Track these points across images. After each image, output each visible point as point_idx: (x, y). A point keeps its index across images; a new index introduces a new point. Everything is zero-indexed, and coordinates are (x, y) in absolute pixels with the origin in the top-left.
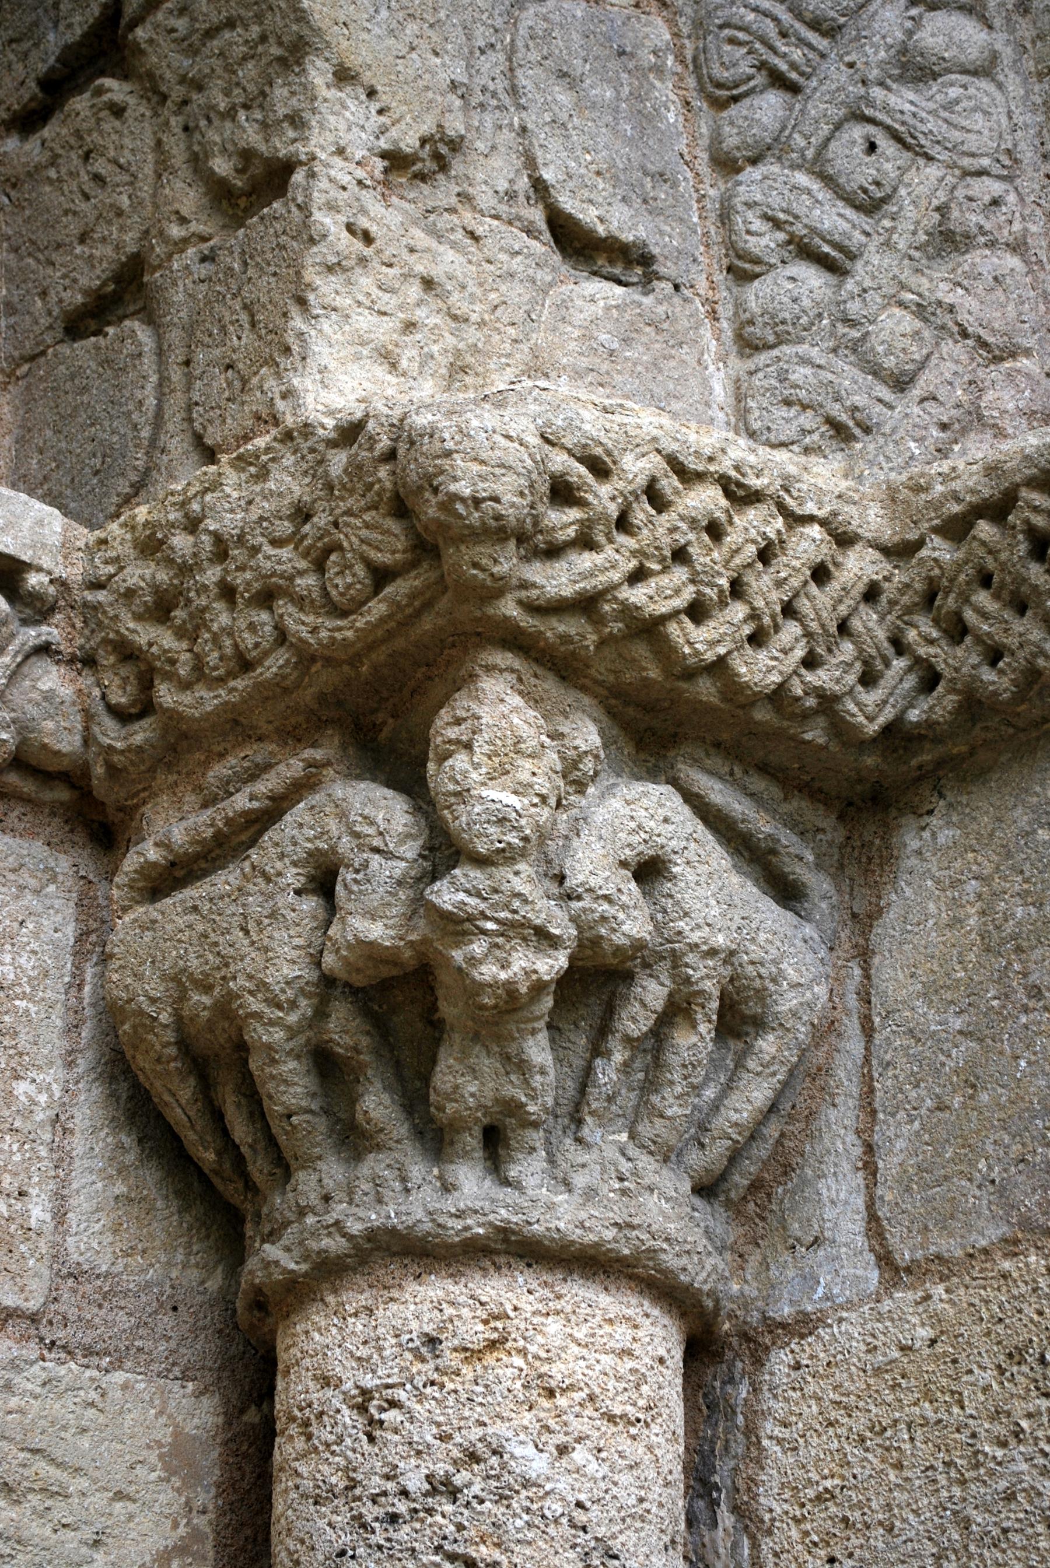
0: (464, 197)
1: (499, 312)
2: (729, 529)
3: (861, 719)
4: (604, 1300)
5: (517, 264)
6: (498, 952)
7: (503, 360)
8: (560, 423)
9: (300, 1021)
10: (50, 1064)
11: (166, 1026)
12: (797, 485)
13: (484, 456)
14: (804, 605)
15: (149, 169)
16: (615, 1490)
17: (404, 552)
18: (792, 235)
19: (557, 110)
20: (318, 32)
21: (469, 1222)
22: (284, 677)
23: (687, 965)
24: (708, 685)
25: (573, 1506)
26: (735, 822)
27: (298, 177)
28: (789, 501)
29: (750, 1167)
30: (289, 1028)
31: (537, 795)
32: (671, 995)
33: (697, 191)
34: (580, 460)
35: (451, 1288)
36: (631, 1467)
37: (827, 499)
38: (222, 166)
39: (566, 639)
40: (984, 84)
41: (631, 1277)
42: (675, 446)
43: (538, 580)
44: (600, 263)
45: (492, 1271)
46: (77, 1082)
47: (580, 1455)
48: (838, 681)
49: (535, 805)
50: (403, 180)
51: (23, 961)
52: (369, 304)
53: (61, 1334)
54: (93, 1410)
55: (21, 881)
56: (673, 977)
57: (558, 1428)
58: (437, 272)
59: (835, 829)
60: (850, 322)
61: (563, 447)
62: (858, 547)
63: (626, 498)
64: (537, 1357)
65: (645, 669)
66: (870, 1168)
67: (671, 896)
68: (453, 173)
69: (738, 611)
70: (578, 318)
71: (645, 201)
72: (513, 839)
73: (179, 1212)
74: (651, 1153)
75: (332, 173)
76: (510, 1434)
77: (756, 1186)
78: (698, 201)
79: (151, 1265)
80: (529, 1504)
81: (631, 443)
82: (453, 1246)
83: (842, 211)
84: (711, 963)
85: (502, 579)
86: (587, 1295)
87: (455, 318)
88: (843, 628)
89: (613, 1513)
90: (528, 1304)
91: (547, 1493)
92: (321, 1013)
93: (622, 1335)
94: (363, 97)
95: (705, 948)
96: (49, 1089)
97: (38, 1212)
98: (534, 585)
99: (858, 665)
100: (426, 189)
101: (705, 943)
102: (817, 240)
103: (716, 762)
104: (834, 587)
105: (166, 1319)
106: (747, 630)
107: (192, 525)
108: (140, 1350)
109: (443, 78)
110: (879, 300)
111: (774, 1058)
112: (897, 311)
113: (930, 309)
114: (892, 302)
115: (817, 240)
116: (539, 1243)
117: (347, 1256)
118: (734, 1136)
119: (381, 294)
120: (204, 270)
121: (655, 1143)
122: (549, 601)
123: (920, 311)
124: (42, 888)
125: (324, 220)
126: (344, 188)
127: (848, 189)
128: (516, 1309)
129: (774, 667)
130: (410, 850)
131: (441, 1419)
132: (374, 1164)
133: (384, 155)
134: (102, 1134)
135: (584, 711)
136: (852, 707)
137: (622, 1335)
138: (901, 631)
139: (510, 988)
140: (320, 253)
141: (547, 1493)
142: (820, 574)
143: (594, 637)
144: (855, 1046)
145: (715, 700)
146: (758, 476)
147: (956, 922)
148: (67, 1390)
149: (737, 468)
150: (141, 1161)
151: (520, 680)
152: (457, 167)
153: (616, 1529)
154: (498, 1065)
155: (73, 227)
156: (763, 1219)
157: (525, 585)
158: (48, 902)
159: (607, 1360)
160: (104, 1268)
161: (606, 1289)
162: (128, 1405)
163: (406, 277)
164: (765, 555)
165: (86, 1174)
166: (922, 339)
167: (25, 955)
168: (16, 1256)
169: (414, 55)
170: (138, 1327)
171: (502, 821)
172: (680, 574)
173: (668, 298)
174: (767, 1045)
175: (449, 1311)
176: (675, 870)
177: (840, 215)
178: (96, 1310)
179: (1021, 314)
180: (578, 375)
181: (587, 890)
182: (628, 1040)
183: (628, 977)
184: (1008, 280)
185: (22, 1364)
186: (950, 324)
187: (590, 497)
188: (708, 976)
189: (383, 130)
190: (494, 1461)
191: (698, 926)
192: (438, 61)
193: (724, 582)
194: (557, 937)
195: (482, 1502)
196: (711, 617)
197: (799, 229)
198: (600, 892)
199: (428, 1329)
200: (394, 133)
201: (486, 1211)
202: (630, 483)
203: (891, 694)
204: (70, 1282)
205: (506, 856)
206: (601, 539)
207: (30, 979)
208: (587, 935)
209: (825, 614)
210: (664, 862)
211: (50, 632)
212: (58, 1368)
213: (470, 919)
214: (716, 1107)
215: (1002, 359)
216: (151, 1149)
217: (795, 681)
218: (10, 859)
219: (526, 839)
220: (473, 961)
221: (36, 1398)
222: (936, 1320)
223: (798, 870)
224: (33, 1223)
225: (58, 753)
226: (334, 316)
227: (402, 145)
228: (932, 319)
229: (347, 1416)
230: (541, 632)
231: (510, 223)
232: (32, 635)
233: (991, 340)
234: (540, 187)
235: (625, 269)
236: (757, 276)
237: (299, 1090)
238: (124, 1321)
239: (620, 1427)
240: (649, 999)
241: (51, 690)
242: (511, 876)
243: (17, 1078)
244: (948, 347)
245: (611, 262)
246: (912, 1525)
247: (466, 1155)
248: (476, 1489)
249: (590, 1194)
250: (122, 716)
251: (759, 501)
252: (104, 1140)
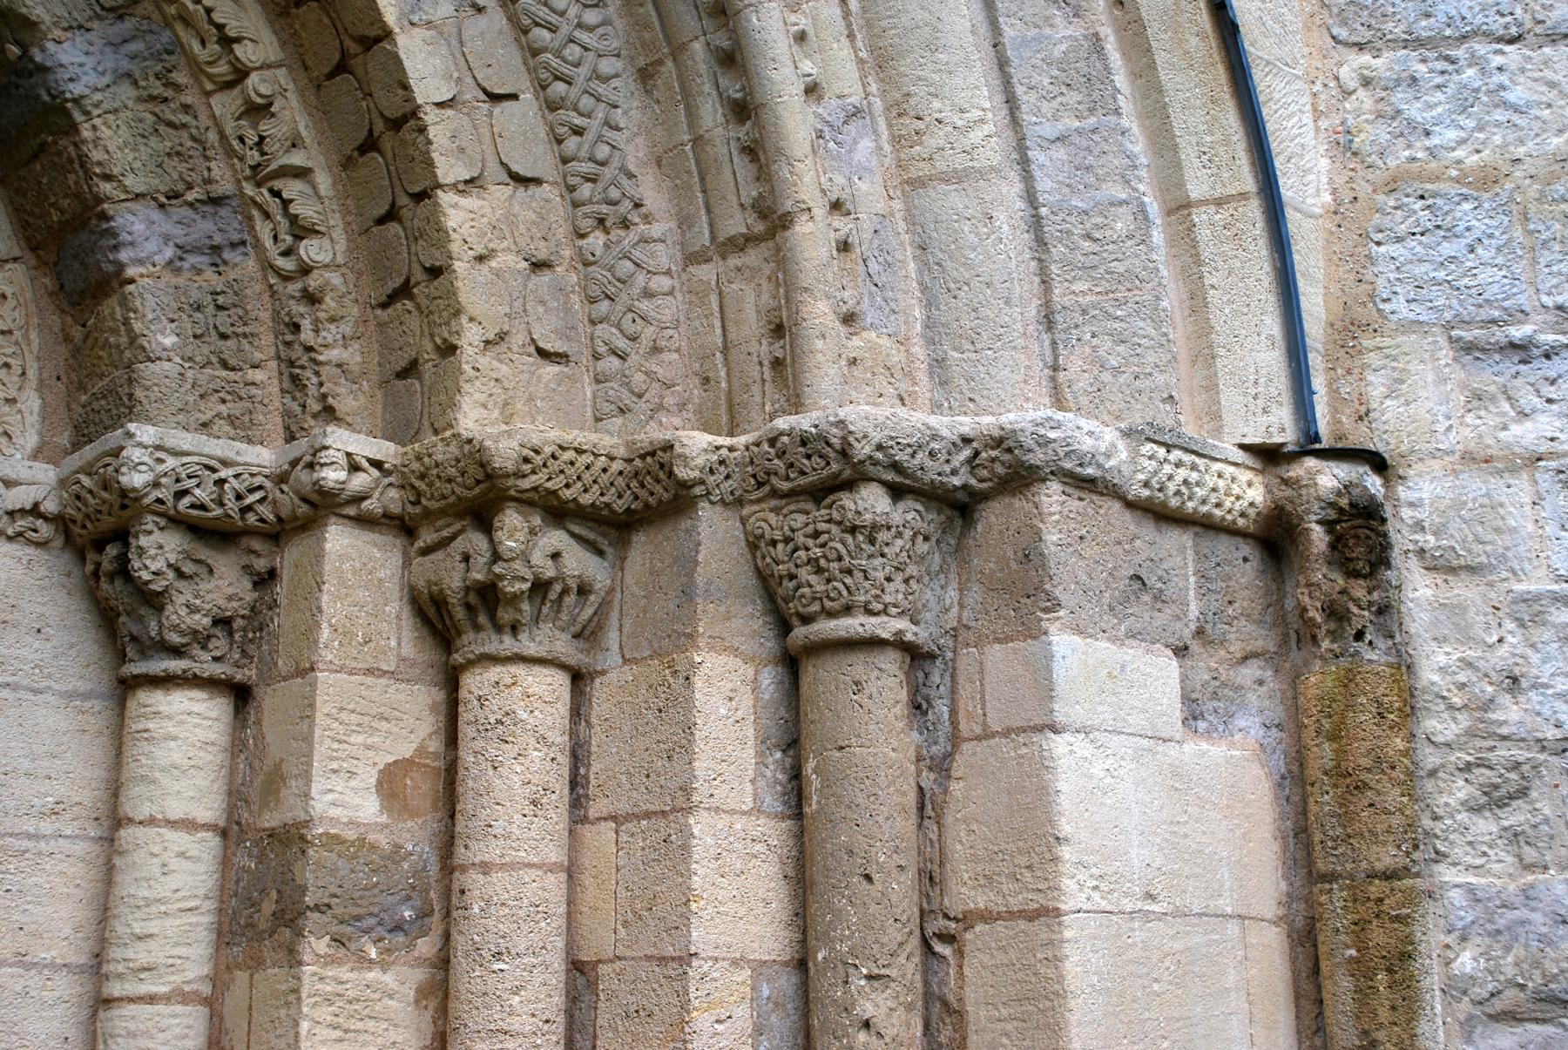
4: (544, 670)
5: (525, 368)
14: (600, 480)
15: (418, 333)
27: (458, 352)
29: (589, 629)
38: (438, 341)
40: (669, 298)
47: (536, 713)
58: (499, 376)
66: (621, 631)
69: (579, 484)
70: (544, 381)
77: (593, 633)
81: (546, 442)
88: (612, 484)
90: (523, 673)
92: (467, 594)
93: (549, 680)
97: (393, 643)
104: (609, 474)
107: (430, 456)
109: (503, 312)
120: (434, 370)
123: (646, 373)
125: (465, 367)
130: (488, 555)
132: (482, 635)
137: (549, 680)
139: (515, 593)
142: (605, 470)
144: (619, 595)
147: (644, 564)
152: (507, 339)
155: (397, 345)
164: (587, 468)
172: (562, 476)
174: (592, 598)
205: (513, 559)
211: (391, 479)
214: (578, 615)
222: (633, 675)
229: (475, 702)
232: (386, 481)
234: (533, 340)
238: (418, 671)
244: (654, 384)
246: (626, 729)
249: (540, 643)
250: (413, 503)
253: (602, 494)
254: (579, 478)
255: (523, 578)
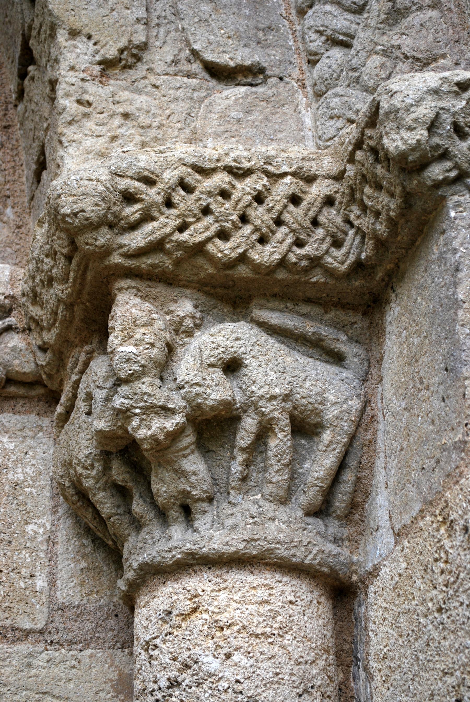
0: (150, 70)
1: (171, 119)
2: (234, 191)
3: (336, 264)
4: (250, 578)
5: (180, 93)
6: (145, 423)
7: (174, 140)
8: (125, 165)
9: (97, 474)
10: (44, 514)
11: (69, 487)
12: (275, 160)
13: (74, 192)
14: (286, 217)
16: (258, 671)
17: (68, 246)
18: (327, 36)
19: (202, 14)
20: (57, 18)
21: (174, 553)
22: (65, 316)
23: (261, 407)
24: (244, 268)
25: (233, 683)
26: (292, 330)
28: (270, 168)
30: (94, 478)
31: (147, 343)
32: (260, 422)
33: (292, 29)
34: (139, 180)
35: (175, 586)
36: (270, 658)
37: (295, 162)
39: (152, 265)
41: (267, 564)
42: (194, 160)
43: (126, 242)
44: (239, 79)
45: (193, 574)
46: (59, 520)
47: (236, 657)
48: (317, 249)
49: (148, 349)
50: (117, 71)
51: (28, 470)
52: (91, 134)
53: (55, 637)
54: (75, 670)
55: (24, 434)
56: (257, 414)
57: (225, 645)
59: (362, 320)
60: (354, 69)
61: (128, 177)
62: (318, 181)
63: (166, 192)
64: (213, 612)
65: (207, 269)
67: (246, 375)
68: (144, 60)
69: (248, 229)
71: (259, 43)
72: (136, 367)
73: (116, 570)
74: (271, 501)
75: (67, 79)
76: (201, 652)
78: (293, 34)
79: (102, 597)
80: (211, 685)
81: (169, 165)
82: (170, 566)
83: (346, 17)
84: (275, 403)
85: (103, 246)
86: (240, 577)
87: (142, 127)
89: (258, 682)
90: (208, 587)
91: (220, 679)
92: (107, 468)
93: (262, 594)
94: (85, 40)
95: (268, 396)
96: (44, 525)
98: (125, 245)
99: (328, 238)
100: (131, 72)
101: (267, 394)
102: (337, 35)
103: (275, 304)
105: (112, 621)
106: (255, 237)
108: (98, 638)
109: (132, 18)
110: (365, 54)
111: (331, 441)
112: (375, 57)
113: (389, 51)
114: (372, 53)
115: (337, 35)
116: (207, 556)
117: (137, 579)
118: (319, 484)
119: (97, 127)
121: (271, 496)
122: (134, 250)
123: (385, 53)
124: (36, 435)
126: (73, 85)
127: (347, 5)
128: (203, 591)
129: (275, 252)
131: (173, 650)
133: (100, 63)
134: (73, 541)
135: (186, 297)
136: (330, 260)
138: (348, 215)
140: (66, 117)
141: (220, 679)
143: (170, 261)
145: (250, 275)
146: (249, 162)
148: (60, 663)
149: (235, 161)
150: (94, 550)
151: (139, 290)
152: (146, 56)
153: (259, 690)
154: (174, 475)
156: (363, 521)
157: (121, 246)
158: (39, 441)
159: (253, 608)
160: (77, 603)
161: (252, 573)
162: (93, 665)
163: (112, 116)
165: (65, 561)
166: (386, 67)
167: (29, 467)
168: (30, 605)
169: (114, 13)
170: (96, 628)
171: (128, 360)
172: (209, 219)
173: (275, 85)
174: (327, 436)
175: (175, 597)
176: (246, 362)
177: (345, 19)
178: (74, 623)
179: (436, 38)
180: (217, 135)
181: (186, 383)
182: (242, 449)
183: (238, 419)
184: (428, 24)
185: (36, 654)
186: (400, 55)
187: (143, 197)
188: (274, 410)
189: (97, 52)
190: (195, 667)
191: (262, 387)
192: (129, 12)
193: (234, 218)
194: (174, 408)
195: (191, 687)
196: (232, 236)
197: (329, 32)
198: (192, 382)
199: (166, 608)
200: (102, 52)
201: (181, 546)
202: (167, 183)
203: (351, 248)
204: (60, 612)
206: (156, 214)
207: (32, 477)
208: (194, 404)
209: (300, 219)
210: (240, 360)
212: (54, 653)
213: (128, 410)
215: (428, 64)
216: (99, 544)
217: (291, 255)
218: (18, 426)
219: (142, 366)
220: (135, 430)
221: (44, 668)
223: (338, 346)
224: (38, 589)
225: (24, 373)
226: (74, 144)
227: (108, 56)
228: (391, 55)
230: (139, 266)
231: (176, 75)
233: (420, 56)
234: (195, 53)
235: (254, 78)
236: (318, 61)
237: (109, 505)
238: (89, 626)
239: (262, 639)
240: (247, 427)
241: (14, 346)
242: (140, 385)
243: (27, 523)
245: (246, 77)
247: (175, 521)
248: (187, 682)
249: (234, 527)
251: (252, 173)
252: (74, 544)
253: (299, 243)
254: (244, 219)
255: (165, 409)
